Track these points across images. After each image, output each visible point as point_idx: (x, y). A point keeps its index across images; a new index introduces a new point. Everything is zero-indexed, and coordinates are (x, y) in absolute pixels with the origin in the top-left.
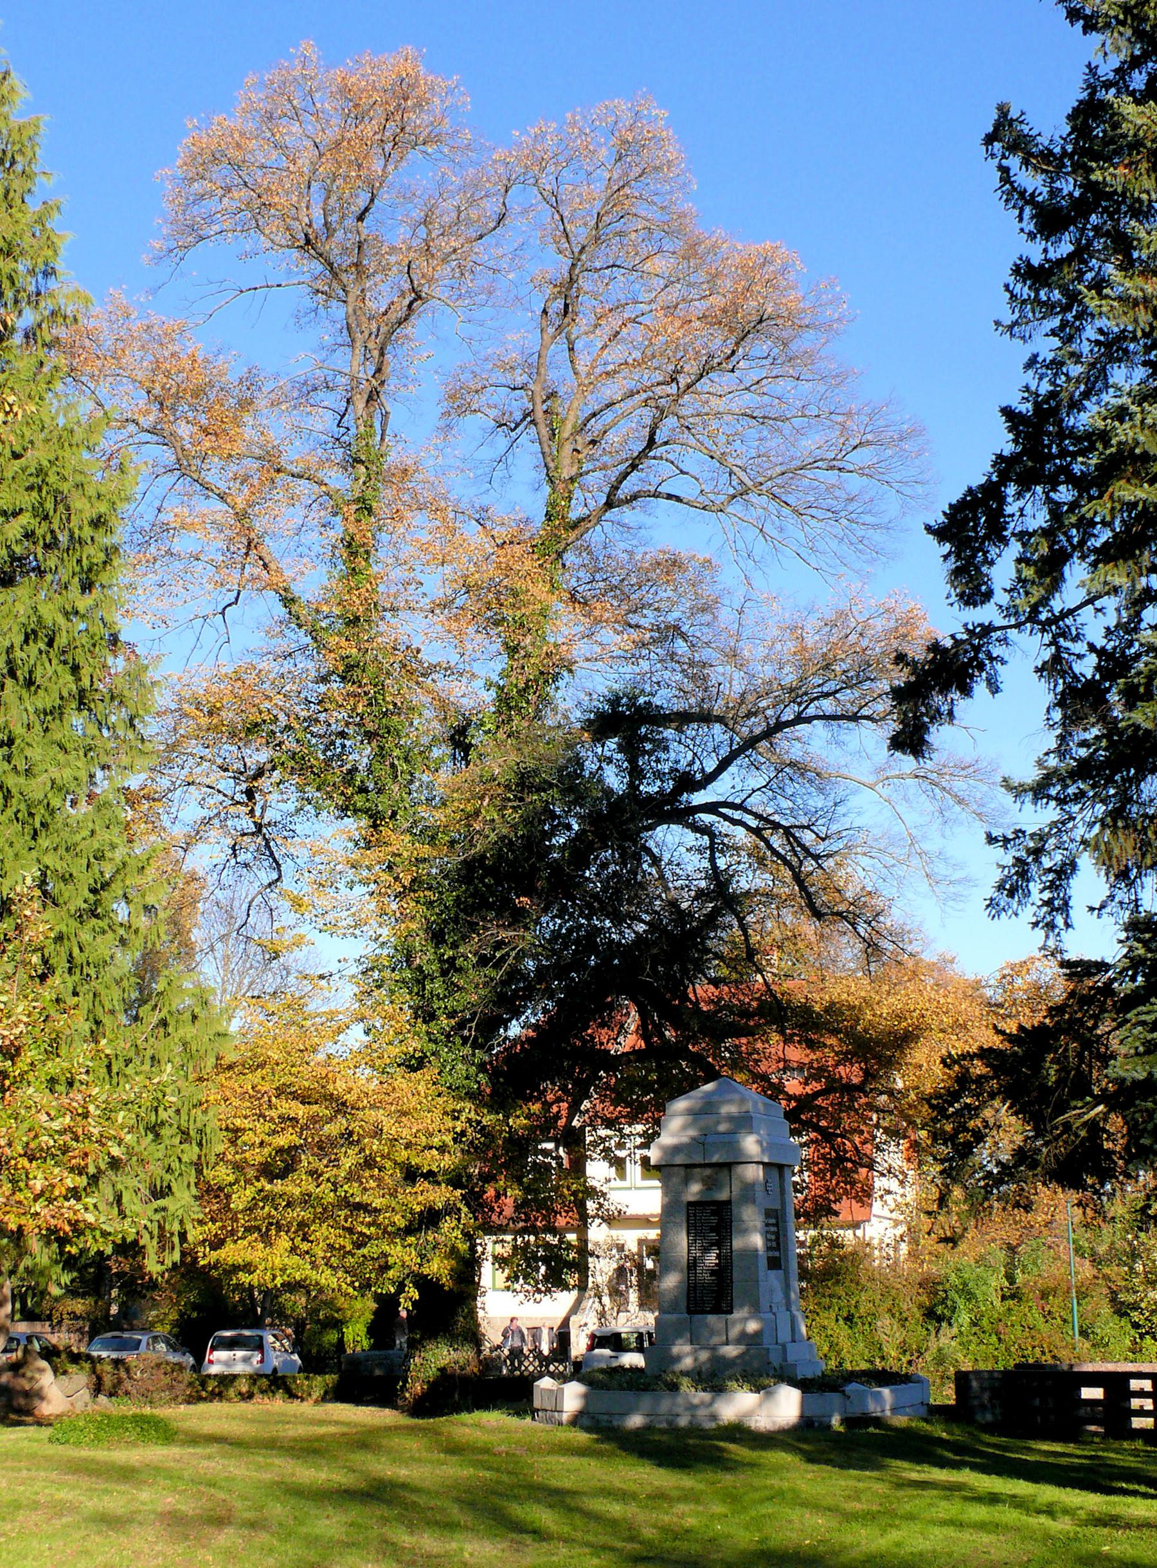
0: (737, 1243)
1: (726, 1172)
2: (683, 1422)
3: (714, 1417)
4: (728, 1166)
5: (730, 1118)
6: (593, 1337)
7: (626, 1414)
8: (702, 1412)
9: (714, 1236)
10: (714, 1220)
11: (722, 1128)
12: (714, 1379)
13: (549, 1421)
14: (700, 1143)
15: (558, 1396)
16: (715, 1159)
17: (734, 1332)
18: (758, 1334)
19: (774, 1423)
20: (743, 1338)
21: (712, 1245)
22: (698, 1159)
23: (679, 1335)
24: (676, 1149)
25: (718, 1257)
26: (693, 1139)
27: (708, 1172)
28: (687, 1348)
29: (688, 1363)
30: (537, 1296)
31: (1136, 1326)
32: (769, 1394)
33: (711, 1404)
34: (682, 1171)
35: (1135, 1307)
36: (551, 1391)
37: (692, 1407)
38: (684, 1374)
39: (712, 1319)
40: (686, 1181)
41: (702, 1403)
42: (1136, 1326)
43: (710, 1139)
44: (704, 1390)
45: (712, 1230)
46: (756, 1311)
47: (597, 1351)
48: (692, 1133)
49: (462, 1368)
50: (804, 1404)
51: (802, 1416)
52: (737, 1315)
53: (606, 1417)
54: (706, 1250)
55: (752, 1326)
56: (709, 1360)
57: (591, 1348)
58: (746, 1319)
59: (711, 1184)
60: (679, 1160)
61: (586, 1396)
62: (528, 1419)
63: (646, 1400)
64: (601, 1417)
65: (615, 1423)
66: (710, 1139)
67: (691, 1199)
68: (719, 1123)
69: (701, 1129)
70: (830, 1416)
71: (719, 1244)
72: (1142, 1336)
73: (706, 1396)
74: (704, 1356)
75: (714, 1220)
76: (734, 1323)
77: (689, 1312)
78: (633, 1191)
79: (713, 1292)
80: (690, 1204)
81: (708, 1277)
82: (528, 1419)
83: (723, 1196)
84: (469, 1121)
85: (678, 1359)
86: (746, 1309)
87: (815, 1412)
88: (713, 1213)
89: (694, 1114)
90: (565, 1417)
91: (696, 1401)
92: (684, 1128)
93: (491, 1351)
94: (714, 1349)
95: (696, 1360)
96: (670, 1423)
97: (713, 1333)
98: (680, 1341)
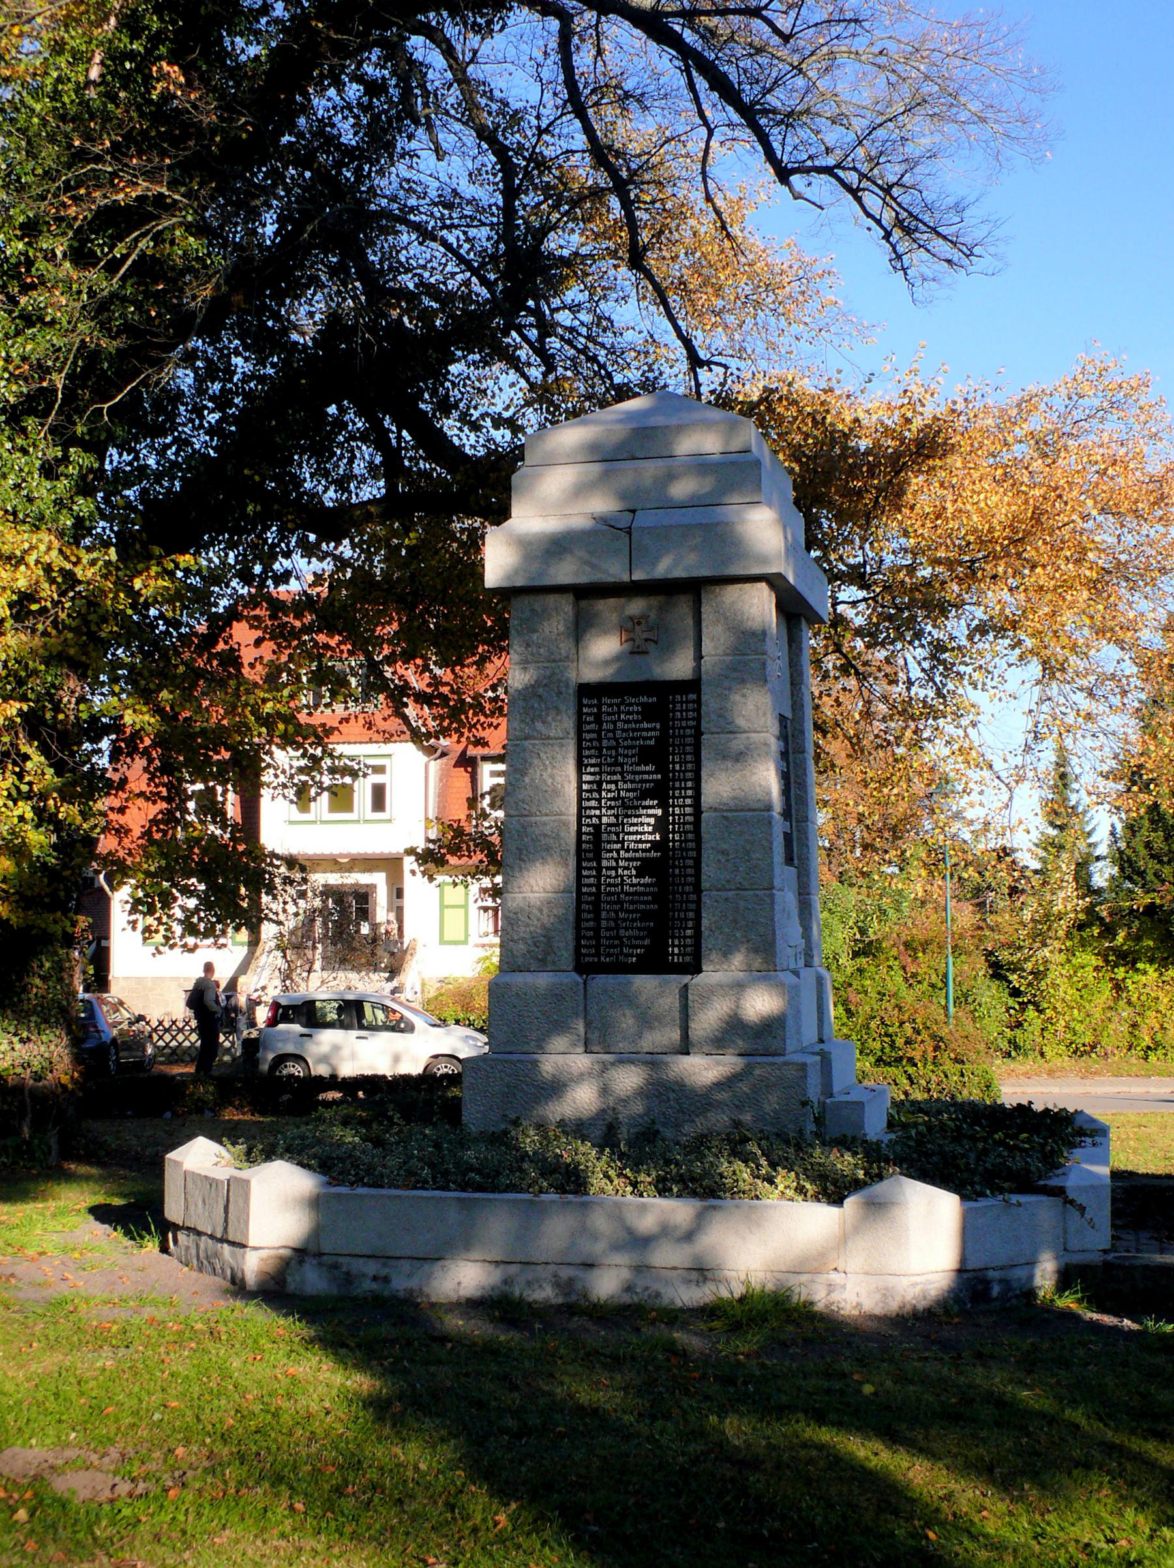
0: (718, 787)
1: (683, 608)
2: (607, 1284)
3: (702, 1272)
4: (693, 589)
5: (701, 465)
6: (276, 1006)
7: (434, 1257)
8: (667, 1256)
9: (649, 773)
10: (651, 732)
11: (682, 489)
12: (682, 1148)
13: (205, 1264)
14: (617, 531)
15: (231, 1199)
16: (666, 567)
17: (709, 1018)
18: (771, 1027)
19: (886, 1293)
20: (735, 1030)
21: (645, 794)
22: (615, 571)
23: (559, 1026)
24: (557, 546)
25: (661, 825)
26: (605, 522)
27: (636, 606)
28: (581, 1061)
29: (583, 1099)
30: (191, 941)
31: (1015, 993)
32: (877, 1207)
33: (689, 1236)
34: (566, 605)
35: (1016, 968)
36: (211, 1182)
37: (640, 1242)
38: (578, 1129)
39: (645, 984)
40: (580, 629)
41: (665, 1231)
42: (1015, 993)
43: (644, 519)
44: (663, 1190)
45: (645, 756)
46: (767, 960)
47: (281, 1026)
48: (602, 504)
49: (38, 1077)
50: (968, 1233)
51: (960, 1271)
52: (713, 974)
53: (371, 1268)
54: (628, 808)
55: (761, 1003)
56: (641, 1093)
57: (272, 1022)
58: (739, 987)
59: (644, 640)
60: (566, 572)
61: (316, 1203)
62: (151, 1246)
63: (498, 1220)
64: (358, 1266)
65: (400, 1284)
66: (644, 519)
67: (591, 675)
68: (671, 477)
69: (623, 496)
70: (1032, 1263)
71: (661, 793)
72: (1023, 1006)
73: (678, 1210)
74: (628, 1080)
75: (651, 732)
76: (710, 993)
77: (582, 968)
78: (318, 827)
79: (646, 916)
80: (585, 690)
81: (630, 876)
82: (151, 1246)
83: (680, 667)
84: (48, 569)
85: (556, 1088)
86: (738, 960)
87: (994, 1253)
88: (648, 713)
89: (609, 457)
90: (253, 1265)
91: (647, 1223)
92: (580, 491)
93: (131, 1024)
94: (653, 1061)
95: (605, 1091)
96: (566, 1286)
97: (647, 1021)
98: (559, 1042)
